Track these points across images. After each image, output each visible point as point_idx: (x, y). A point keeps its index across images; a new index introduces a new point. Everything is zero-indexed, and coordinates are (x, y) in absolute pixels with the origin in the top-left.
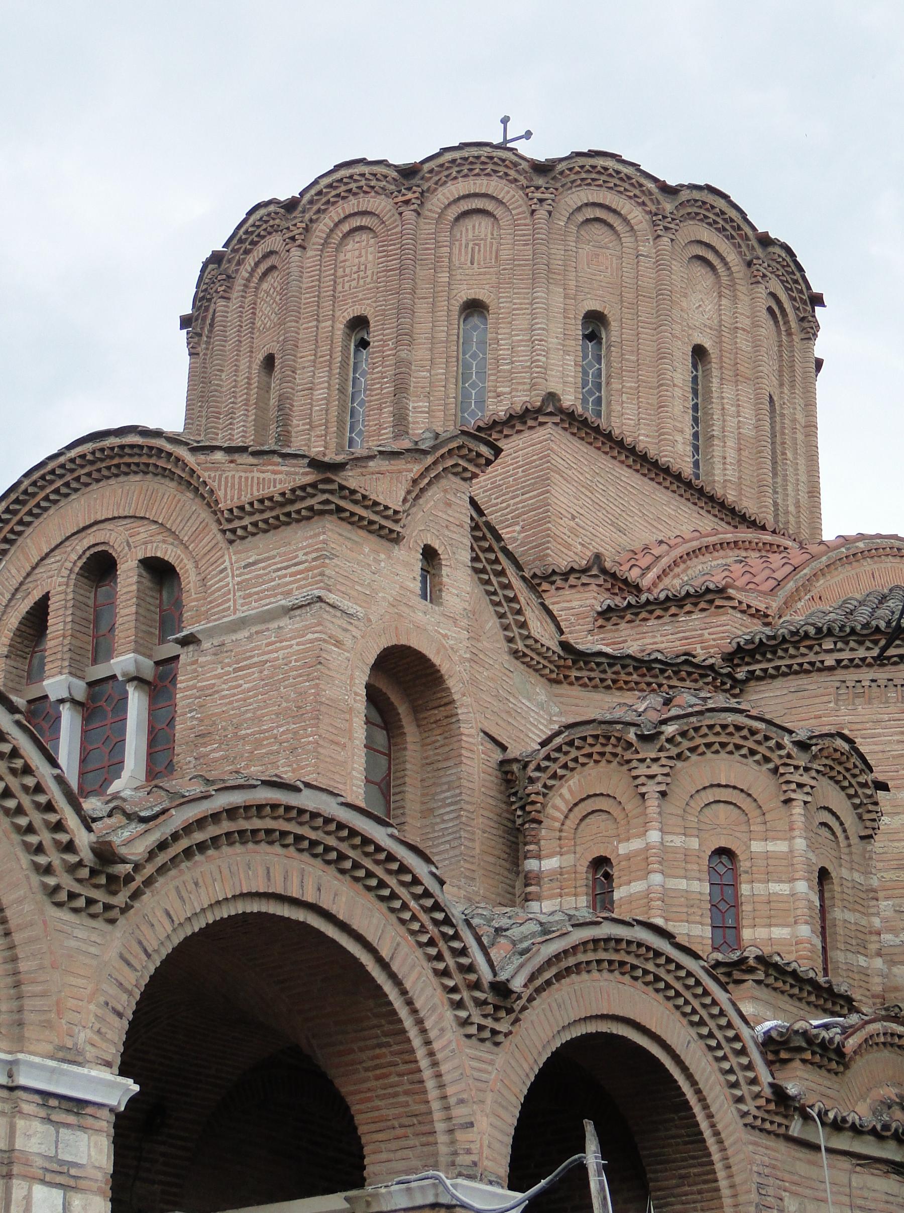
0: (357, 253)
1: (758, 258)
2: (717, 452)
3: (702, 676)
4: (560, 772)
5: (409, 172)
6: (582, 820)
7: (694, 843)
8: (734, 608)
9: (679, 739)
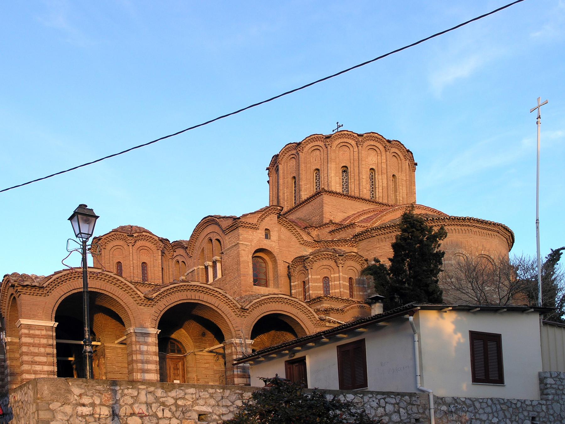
2: (377, 191)
7: (319, 277)
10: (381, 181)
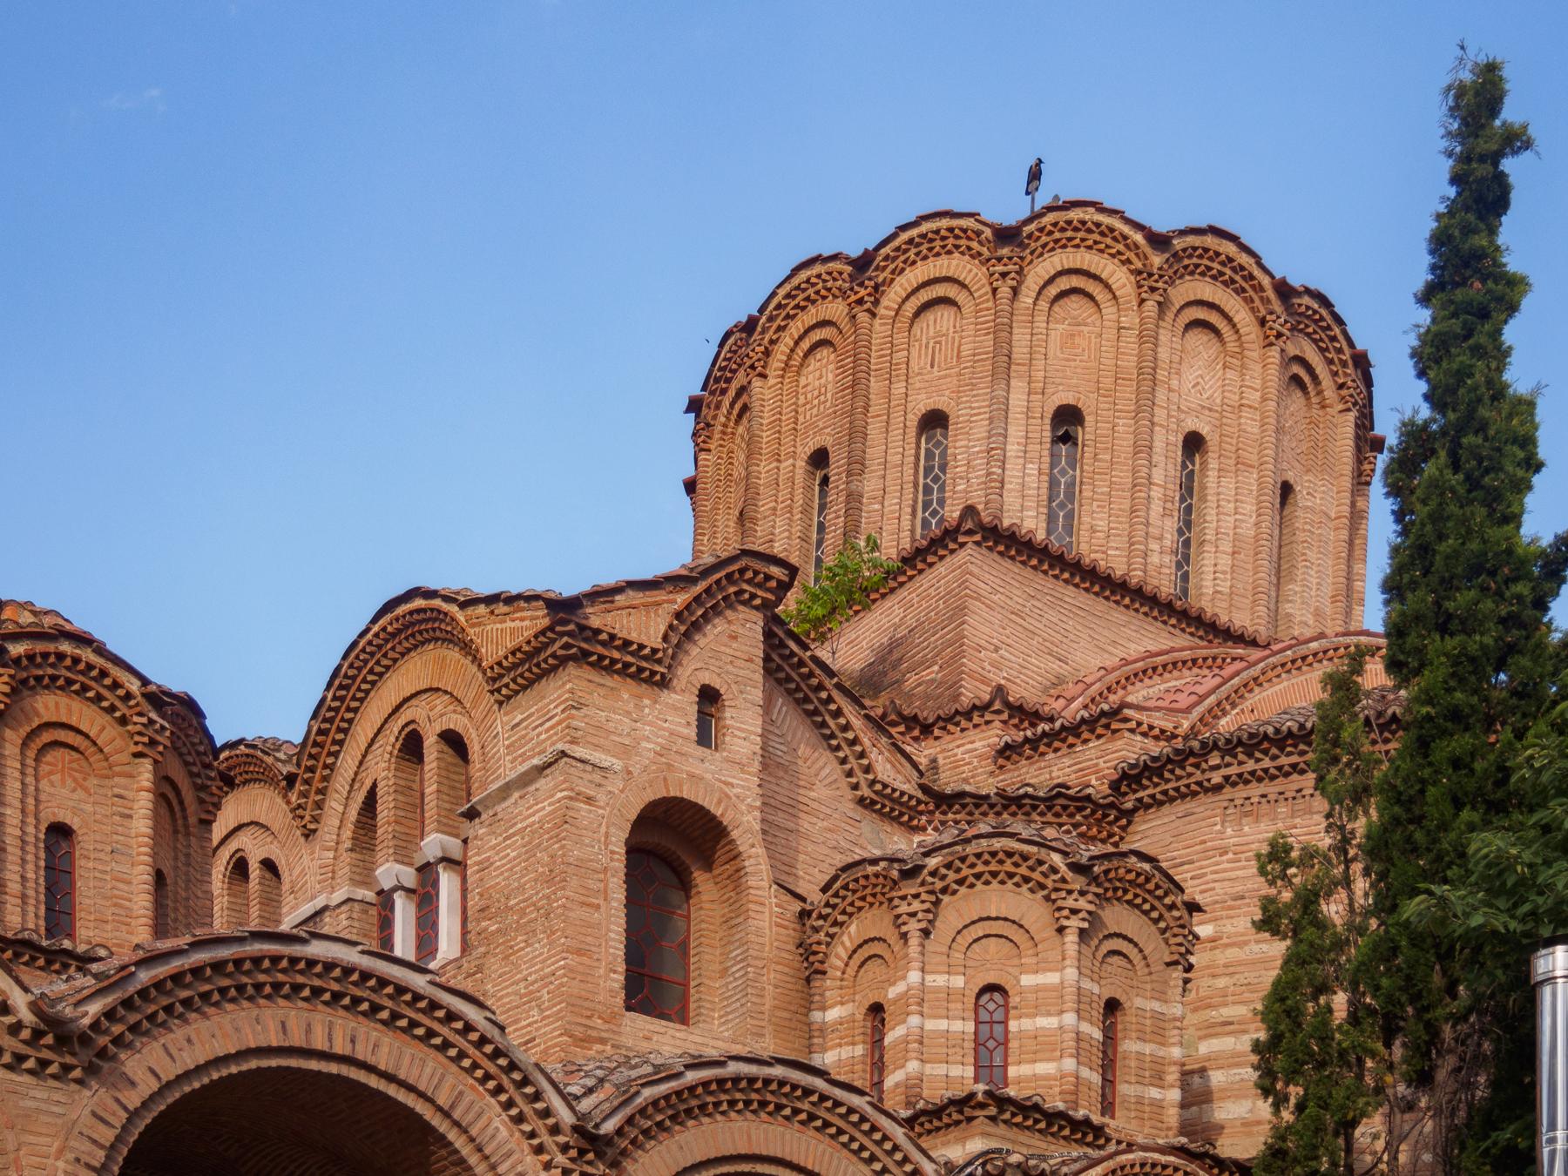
0: (817, 374)
1: (1271, 313)
3: (1080, 809)
4: (841, 918)
5: (863, 263)
6: (860, 967)
7: (958, 981)
8: (1132, 731)
9: (943, 871)
10: (1233, 504)
